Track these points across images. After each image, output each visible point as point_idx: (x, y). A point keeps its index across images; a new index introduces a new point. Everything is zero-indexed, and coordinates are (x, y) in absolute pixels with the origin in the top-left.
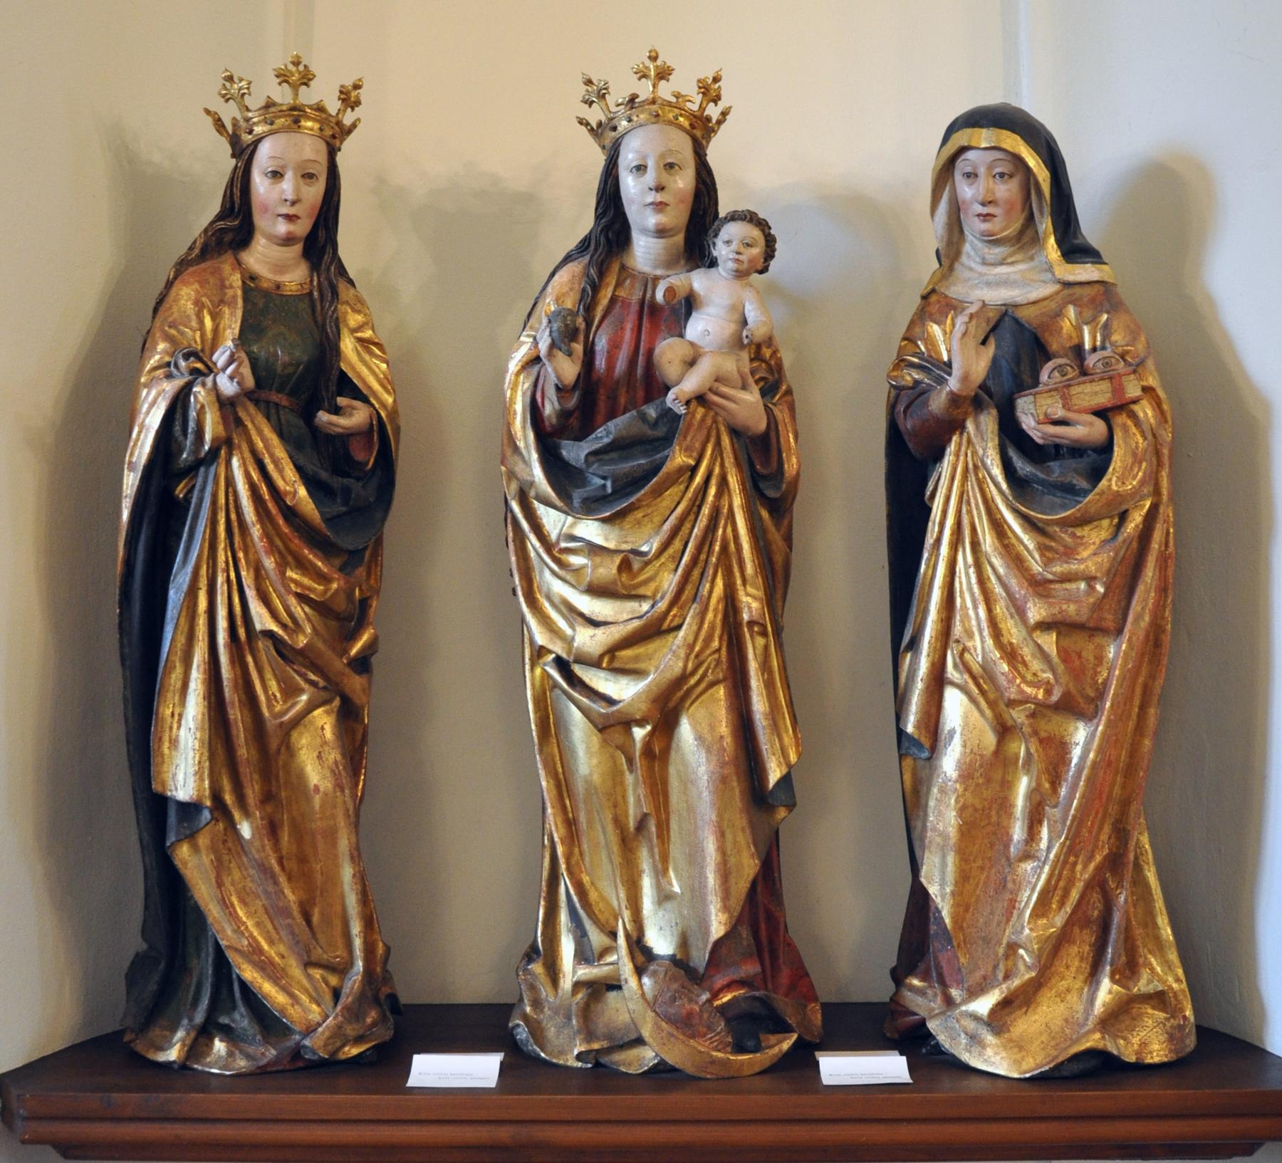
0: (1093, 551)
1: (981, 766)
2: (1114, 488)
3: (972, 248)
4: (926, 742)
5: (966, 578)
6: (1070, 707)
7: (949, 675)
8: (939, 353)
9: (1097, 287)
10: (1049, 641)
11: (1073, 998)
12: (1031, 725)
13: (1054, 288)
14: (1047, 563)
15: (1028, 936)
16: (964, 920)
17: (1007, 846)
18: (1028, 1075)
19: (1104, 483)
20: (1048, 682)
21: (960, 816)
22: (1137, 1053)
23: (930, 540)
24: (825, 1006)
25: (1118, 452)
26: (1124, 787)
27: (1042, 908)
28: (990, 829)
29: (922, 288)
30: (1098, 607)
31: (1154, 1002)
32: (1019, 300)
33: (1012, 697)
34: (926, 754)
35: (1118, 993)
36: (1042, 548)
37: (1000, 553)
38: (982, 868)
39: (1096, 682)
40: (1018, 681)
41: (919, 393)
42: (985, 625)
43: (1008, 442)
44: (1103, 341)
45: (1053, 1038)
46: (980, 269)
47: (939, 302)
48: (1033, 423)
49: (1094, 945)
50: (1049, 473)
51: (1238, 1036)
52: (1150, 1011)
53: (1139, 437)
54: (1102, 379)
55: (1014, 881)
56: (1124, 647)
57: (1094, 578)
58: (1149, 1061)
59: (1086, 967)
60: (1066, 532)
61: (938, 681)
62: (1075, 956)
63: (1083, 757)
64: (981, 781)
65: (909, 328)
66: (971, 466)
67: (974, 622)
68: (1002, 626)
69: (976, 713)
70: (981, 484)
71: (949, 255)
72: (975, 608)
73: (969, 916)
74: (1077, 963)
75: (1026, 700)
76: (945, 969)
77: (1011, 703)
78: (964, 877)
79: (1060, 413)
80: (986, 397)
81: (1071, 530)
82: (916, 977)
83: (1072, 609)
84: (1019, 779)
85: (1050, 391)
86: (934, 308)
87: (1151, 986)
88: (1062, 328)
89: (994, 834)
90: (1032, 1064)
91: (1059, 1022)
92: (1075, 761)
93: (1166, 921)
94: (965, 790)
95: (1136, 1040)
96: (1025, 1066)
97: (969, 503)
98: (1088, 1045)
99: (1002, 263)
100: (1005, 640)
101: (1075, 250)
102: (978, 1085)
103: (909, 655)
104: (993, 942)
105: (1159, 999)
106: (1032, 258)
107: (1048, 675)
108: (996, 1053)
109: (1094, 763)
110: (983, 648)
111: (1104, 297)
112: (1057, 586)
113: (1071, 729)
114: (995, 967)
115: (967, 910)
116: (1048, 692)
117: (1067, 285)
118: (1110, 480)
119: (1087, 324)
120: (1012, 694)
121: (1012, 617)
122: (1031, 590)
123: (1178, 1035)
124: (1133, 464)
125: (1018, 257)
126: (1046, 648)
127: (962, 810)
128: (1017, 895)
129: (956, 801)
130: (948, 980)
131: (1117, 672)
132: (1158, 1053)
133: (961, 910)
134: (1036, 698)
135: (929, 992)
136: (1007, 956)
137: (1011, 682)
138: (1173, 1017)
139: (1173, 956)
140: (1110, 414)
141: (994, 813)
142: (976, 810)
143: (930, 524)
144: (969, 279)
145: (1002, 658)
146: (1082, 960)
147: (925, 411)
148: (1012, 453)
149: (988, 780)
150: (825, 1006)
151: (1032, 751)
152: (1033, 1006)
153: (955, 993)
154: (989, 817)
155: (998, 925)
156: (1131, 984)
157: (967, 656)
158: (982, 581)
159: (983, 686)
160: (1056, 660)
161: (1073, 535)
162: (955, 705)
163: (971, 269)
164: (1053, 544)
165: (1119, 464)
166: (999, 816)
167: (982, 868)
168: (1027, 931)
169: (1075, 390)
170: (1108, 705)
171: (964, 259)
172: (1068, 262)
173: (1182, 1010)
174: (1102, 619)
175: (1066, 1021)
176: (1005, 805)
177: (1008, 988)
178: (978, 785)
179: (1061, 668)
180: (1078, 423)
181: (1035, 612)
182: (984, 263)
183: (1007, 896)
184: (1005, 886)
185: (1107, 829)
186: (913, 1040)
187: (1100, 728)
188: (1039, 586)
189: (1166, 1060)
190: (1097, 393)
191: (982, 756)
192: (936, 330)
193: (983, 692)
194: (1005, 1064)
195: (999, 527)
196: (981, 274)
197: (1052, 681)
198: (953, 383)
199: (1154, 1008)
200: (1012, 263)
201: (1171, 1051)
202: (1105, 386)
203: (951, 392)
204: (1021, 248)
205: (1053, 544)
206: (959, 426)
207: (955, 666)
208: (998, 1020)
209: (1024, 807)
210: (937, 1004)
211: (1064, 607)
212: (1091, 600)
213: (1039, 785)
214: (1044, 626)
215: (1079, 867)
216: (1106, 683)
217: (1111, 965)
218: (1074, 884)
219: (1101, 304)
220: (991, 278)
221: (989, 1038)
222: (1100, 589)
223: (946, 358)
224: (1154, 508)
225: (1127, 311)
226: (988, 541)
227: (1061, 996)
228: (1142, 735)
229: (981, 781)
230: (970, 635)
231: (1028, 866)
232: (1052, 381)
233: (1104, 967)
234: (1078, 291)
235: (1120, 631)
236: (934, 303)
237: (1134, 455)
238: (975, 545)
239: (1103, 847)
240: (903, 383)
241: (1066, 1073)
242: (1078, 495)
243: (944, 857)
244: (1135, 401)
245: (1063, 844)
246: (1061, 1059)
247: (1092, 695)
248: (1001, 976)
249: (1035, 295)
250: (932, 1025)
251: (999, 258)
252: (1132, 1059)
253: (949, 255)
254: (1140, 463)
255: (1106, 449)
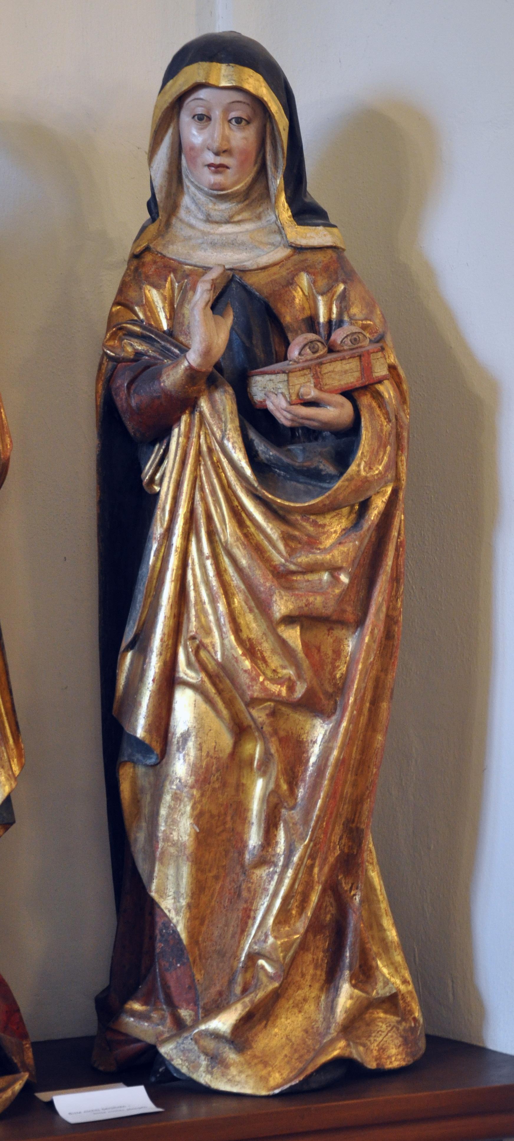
0: (336, 540)
1: (217, 770)
2: (363, 473)
3: (192, 205)
4: (157, 748)
5: (201, 573)
6: (313, 705)
7: (181, 675)
8: (158, 321)
9: (330, 251)
10: (293, 635)
11: (310, 1007)
12: (271, 724)
13: (281, 253)
14: (292, 552)
15: (273, 945)
16: (199, 933)
17: (241, 853)
18: (277, 1091)
19: (353, 468)
20: (289, 679)
21: (197, 824)
22: (378, 1059)
23: (158, 530)
24: (34, 1045)
25: (366, 434)
26: (355, 785)
27: (284, 917)
28: (225, 836)
29: (125, 247)
30: (341, 599)
31: (385, 1006)
32: (249, 264)
33: (255, 695)
34: (153, 760)
35: (358, 998)
36: (287, 538)
37: (243, 544)
38: (217, 878)
39: (334, 678)
40: (261, 679)
41: (144, 369)
42: (224, 620)
43: (248, 425)
44: (340, 314)
45: (296, 1051)
46: (202, 226)
47: (155, 262)
48: (284, 404)
49: (328, 950)
50: (293, 458)
51: (451, 1037)
52: (382, 1015)
53: (382, 419)
54: (352, 357)
55: (249, 890)
56: (367, 639)
57: (339, 569)
58: (389, 1066)
59: (322, 975)
60: (307, 520)
61: (169, 681)
62: (311, 968)
63: (325, 755)
64: (217, 785)
65: (121, 291)
66: (204, 448)
67: (211, 618)
68: (241, 621)
69: (212, 714)
70: (217, 466)
71: (161, 210)
72: (213, 601)
73: (204, 929)
74: (311, 971)
75: (270, 697)
76: (173, 989)
77: (252, 702)
78: (199, 888)
79: (313, 393)
80: (219, 375)
81: (312, 517)
82: (138, 1000)
83: (318, 600)
84: (254, 783)
85: (303, 369)
86: (151, 270)
87: (387, 989)
88: (294, 298)
89: (229, 840)
90: (278, 1079)
91: (299, 1033)
92: (313, 759)
93: (391, 922)
94: (202, 795)
95: (374, 1046)
96: (272, 1083)
97: (202, 489)
98: (336, 1053)
99: (228, 221)
100: (244, 635)
101: (306, 212)
102: (219, 1106)
103: (129, 655)
104: (228, 955)
105: (392, 1002)
106: (259, 217)
107: (290, 672)
108: (241, 1072)
109: (340, 763)
110: (223, 645)
111: (334, 265)
112: (299, 578)
113: (308, 727)
114: (231, 981)
115: (202, 923)
116: (291, 689)
117: (298, 249)
118: (359, 465)
119: (322, 294)
120: (256, 692)
121: (251, 611)
122: (276, 583)
123: (411, 1038)
124: (379, 447)
125: (245, 215)
126: (291, 642)
127: (198, 818)
128: (252, 904)
129: (193, 808)
130: (176, 1000)
131: (360, 666)
132: (395, 1058)
133: (197, 922)
134: (279, 694)
135: (155, 1015)
136: (246, 968)
137: (254, 679)
138: (404, 1019)
139: (399, 958)
140: (356, 394)
141: (229, 818)
142: (212, 816)
143: (158, 512)
144: (190, 238)
145: (244, 654)
146: (316, 967)
147: (156, 387)
148: (253, 435)
149: (224, 784)
150: (34, 1045)
151: (273, 751)
152: (272, 1019)
153: (185, 1013)
154: (224, 823)
155: (233, 936)
156: (369, 988)
157: (203, 654)
158: (220, 573)
159: (220, 684)
160: (301, 655)
161: (315, 524)
162: (186, 707)
163: (191, 226)
164: (297, 533)
165: (367, 448)
166: (234, 822)
167: (217, 878)
168: (271, 940)
169: (327, 368)
170: (351, 700)
171: (182, 213)
172: (299, 224)
173: (411, 1012)
174: (344, 611)
175: (306, 1031)
176: (240, 810)
177: (251, 1001)
178: (214, 790)
179: (306, 664)
180: (330, 404)
181: (282, 606)
182: (209, 220)
183: (242, 905)
184: (239, 895)
185: (338, 829)
186: (142, 1066)
187: (344, 724)
188: (283, 577)
189: (403, 1063)
190: (344, 372)
191: (218, 759)
192: (154, 295)
193: (219, 692)
194: (251, 1082)
195: (238, 513)
196: (204, 233)
197: (294, 678)
198: (193, 358)
199: (386, 1012)
200: (239, 222)
201: (407, 1054)
202: (354, 364)
203: (190, 368)
204: (249, 205)
205: (297, 533)
206: (190, 404)
207: (189, 664)
208: (240, 1037)
209: (260, 811)
210: (166, 1028)
211: (311, 599)
212: (337, 591)
213: (278, 786)
214: (289, 620)
215: (316, 870)
216: (346, 678)
217: (350, 970)
218: (312, 888)
219: (336, 273)
220: (217, 238)
221: (232, 1056)
222: (344, 578)
223: (165, 326)
224: (395, 492)
225: (360, 282)
226: (228, 531)
227: (299, 1007)
228: (374, 730)
229: (217, 785)
230: (208, 632)
231: (263, 872)
232: (303, 358)
233: (342, 971)
234: (309, 256)
235: (360, 623)
236: (144, 264)
237: (380, 438)
238: (212, 534)
239: (334, 848)
240: (122, 355)
241: (314, 1085)
242: (324, 481)
243: (178, 869)
244: (380, 381)
245: (307, 846)
246: (310, 1070)
247: (331, 690)
248: (238, 989)
249: (264, 260)
250: (165, 1050)
251: (226, 215)
252: (372, 1065)
253: (161, 210)
254: (385, 447)
255: (353, 430)
